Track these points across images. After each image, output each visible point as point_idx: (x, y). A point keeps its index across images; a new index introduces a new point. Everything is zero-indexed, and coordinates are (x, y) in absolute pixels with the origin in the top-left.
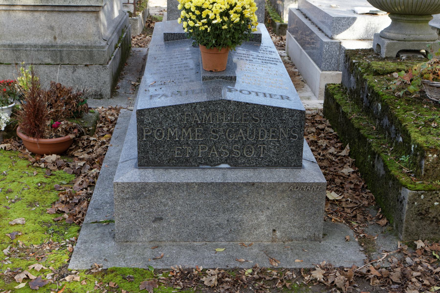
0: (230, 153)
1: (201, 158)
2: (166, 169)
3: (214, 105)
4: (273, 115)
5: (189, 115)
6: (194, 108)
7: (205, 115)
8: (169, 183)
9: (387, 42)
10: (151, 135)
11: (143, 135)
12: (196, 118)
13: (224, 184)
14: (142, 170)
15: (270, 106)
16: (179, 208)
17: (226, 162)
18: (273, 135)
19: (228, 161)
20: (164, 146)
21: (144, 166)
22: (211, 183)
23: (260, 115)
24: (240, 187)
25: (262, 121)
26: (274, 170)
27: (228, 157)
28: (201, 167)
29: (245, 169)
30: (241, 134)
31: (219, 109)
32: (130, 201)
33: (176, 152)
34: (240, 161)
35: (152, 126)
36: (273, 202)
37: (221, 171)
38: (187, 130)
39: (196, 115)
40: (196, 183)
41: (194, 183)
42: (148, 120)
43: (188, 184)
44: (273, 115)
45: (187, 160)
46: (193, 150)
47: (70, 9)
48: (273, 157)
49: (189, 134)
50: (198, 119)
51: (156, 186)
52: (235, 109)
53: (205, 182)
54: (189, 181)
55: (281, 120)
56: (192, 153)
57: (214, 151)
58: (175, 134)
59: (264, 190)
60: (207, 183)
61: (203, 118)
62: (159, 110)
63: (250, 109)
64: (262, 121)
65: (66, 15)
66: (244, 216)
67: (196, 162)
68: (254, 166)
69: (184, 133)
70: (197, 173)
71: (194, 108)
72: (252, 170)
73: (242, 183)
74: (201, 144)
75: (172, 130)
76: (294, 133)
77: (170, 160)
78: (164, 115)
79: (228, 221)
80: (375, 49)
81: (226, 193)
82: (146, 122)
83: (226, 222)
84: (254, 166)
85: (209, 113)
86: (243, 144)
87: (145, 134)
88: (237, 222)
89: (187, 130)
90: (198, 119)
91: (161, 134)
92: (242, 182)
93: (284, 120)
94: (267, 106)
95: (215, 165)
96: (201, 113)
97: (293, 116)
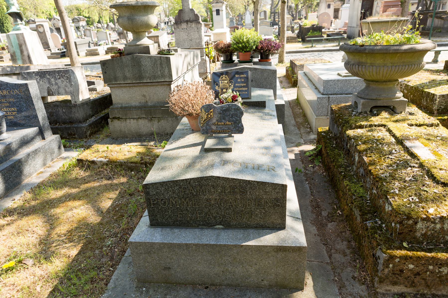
0: (223, 217)
1: (199, 221)
2: (172, 228)
3: (205, 180)
4: (257, 188)
5: (186, 188)
6: (189, 183)
7: (199, 188)
8: (171, 243)
9: (362, 101)
10: (156, 203)
11: (150, 203)
12: (192, 191)
13: (216, 245)
14: (152, 229)
15: (254, 181)
16: (182, 261)
17: (220, 224)
18: (258, 204)
19: (222, 223)
20: (168, 212)
21: (155, 225)
22: (206, 245)
23: (246, 188)
24: (231, 248)
25: (248, 193)
26: (261, 231)
27: (222, 220)
28: (200, 227)
29: (237, 230)
30: (231, 203)
31: (210, 184)
32: (143, 255)
33: (179, 216)
34: (232, 224)
35: (157, 197)
36: (260, 260)
37: (217, 231)
38: (185, 200)
39: (191, 188)
40: (193, 244)
41: (191, 244)
42: (152, 192)
43: (186, 245)
44: (257, 188)
45: (188, 222)
46: (192, 214)
47: (154, 84)
48: (260, 221)
49: (187, 202)
50: (193, 191)
51: (162, 246)
52: (224, 183)
53: (201, 243)
54: (188, 242)
55: (265, 192)
56: (192, 217)
57: (209, 216)
58: (176, 202)
59: (252, 251)
60: (202, 244)
61: (197, 191)
62: (160, 184)
63: (237, 184)
64: (248, 193)
65: (152, 87)
66: (236, 269)
67: (196, 223)
68: (244, 227)
69: (183, 202)
70: (196, 234)
71: (189, 183)
72: (242, 231)
73: (232, 245)
74: (198, 210)
75: (174, 200)
76: (277, 202)
77: (175, 221)
78: (165, 188)
79: (223, 272)
80: (353, 104)
81: (219, 252)
82: (151, 193)
83: (222, 273)
84: (244, 227)
85: (202, 187)
86: (233, 211)
87: (152, 202)
88: (230, 273)
89: (185, 200)
90: (193, 191)
91: (165, 202)
92: (232, 244)
93: (268, 192)
94: (252, 181)
95: (211, 226)
96: (195, 187)
97: (275, 189)
